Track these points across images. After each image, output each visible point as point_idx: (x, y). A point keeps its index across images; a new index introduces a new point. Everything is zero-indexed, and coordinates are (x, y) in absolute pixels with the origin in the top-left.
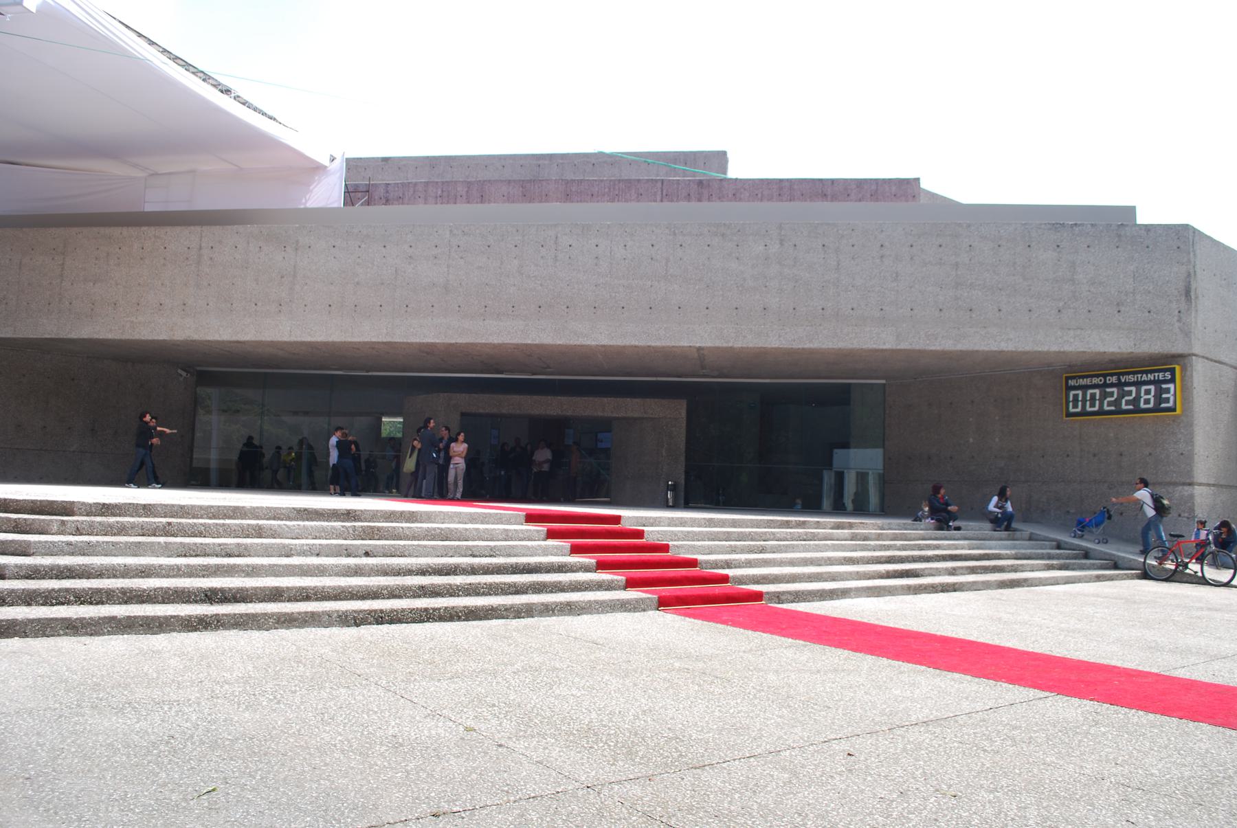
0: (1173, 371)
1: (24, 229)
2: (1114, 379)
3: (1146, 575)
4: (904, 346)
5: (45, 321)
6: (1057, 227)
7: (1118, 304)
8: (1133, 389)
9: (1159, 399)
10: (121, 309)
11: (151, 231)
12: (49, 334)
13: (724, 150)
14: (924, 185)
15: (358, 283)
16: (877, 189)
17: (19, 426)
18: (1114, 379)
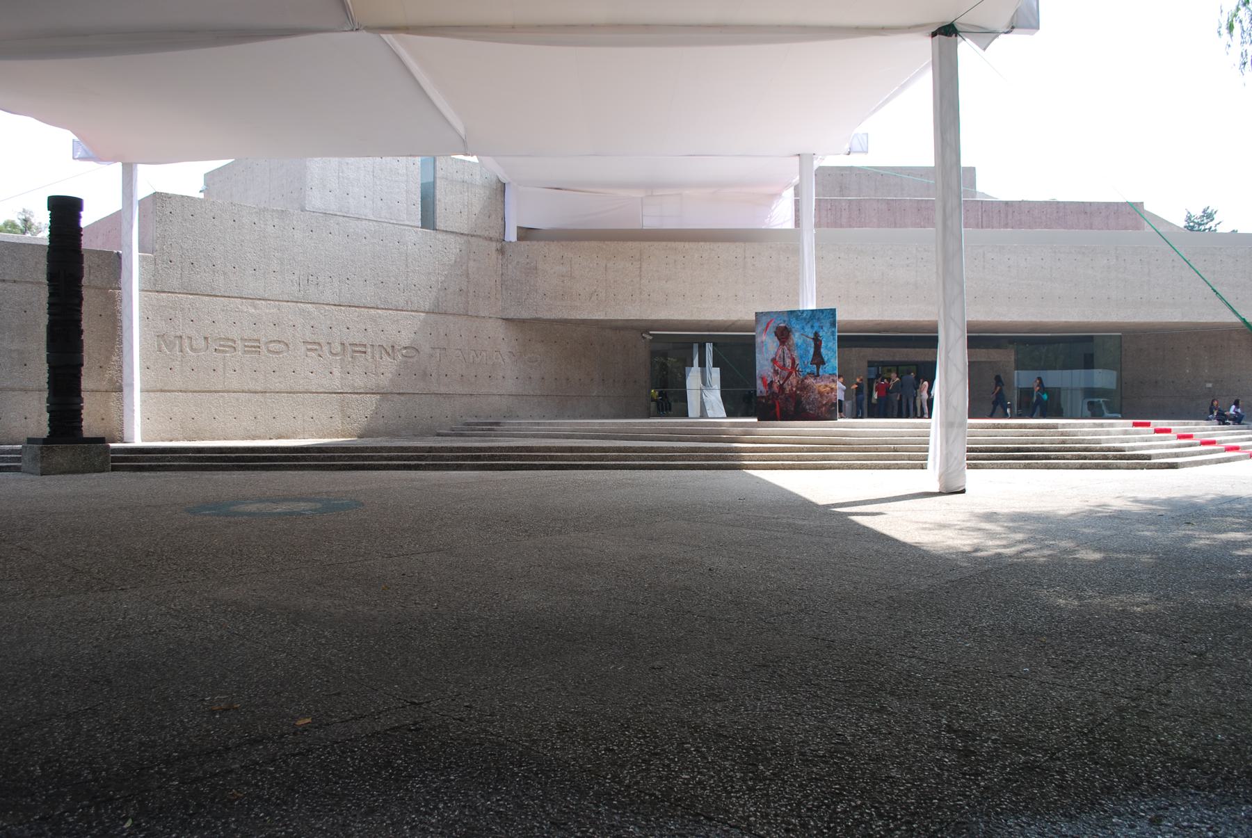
1: (606, 242)
4: (1186, 320)
10: (689, 299)
11: (707, 245)
13: (973, 166)
14: (1147, 207)
16: (1118, 210)
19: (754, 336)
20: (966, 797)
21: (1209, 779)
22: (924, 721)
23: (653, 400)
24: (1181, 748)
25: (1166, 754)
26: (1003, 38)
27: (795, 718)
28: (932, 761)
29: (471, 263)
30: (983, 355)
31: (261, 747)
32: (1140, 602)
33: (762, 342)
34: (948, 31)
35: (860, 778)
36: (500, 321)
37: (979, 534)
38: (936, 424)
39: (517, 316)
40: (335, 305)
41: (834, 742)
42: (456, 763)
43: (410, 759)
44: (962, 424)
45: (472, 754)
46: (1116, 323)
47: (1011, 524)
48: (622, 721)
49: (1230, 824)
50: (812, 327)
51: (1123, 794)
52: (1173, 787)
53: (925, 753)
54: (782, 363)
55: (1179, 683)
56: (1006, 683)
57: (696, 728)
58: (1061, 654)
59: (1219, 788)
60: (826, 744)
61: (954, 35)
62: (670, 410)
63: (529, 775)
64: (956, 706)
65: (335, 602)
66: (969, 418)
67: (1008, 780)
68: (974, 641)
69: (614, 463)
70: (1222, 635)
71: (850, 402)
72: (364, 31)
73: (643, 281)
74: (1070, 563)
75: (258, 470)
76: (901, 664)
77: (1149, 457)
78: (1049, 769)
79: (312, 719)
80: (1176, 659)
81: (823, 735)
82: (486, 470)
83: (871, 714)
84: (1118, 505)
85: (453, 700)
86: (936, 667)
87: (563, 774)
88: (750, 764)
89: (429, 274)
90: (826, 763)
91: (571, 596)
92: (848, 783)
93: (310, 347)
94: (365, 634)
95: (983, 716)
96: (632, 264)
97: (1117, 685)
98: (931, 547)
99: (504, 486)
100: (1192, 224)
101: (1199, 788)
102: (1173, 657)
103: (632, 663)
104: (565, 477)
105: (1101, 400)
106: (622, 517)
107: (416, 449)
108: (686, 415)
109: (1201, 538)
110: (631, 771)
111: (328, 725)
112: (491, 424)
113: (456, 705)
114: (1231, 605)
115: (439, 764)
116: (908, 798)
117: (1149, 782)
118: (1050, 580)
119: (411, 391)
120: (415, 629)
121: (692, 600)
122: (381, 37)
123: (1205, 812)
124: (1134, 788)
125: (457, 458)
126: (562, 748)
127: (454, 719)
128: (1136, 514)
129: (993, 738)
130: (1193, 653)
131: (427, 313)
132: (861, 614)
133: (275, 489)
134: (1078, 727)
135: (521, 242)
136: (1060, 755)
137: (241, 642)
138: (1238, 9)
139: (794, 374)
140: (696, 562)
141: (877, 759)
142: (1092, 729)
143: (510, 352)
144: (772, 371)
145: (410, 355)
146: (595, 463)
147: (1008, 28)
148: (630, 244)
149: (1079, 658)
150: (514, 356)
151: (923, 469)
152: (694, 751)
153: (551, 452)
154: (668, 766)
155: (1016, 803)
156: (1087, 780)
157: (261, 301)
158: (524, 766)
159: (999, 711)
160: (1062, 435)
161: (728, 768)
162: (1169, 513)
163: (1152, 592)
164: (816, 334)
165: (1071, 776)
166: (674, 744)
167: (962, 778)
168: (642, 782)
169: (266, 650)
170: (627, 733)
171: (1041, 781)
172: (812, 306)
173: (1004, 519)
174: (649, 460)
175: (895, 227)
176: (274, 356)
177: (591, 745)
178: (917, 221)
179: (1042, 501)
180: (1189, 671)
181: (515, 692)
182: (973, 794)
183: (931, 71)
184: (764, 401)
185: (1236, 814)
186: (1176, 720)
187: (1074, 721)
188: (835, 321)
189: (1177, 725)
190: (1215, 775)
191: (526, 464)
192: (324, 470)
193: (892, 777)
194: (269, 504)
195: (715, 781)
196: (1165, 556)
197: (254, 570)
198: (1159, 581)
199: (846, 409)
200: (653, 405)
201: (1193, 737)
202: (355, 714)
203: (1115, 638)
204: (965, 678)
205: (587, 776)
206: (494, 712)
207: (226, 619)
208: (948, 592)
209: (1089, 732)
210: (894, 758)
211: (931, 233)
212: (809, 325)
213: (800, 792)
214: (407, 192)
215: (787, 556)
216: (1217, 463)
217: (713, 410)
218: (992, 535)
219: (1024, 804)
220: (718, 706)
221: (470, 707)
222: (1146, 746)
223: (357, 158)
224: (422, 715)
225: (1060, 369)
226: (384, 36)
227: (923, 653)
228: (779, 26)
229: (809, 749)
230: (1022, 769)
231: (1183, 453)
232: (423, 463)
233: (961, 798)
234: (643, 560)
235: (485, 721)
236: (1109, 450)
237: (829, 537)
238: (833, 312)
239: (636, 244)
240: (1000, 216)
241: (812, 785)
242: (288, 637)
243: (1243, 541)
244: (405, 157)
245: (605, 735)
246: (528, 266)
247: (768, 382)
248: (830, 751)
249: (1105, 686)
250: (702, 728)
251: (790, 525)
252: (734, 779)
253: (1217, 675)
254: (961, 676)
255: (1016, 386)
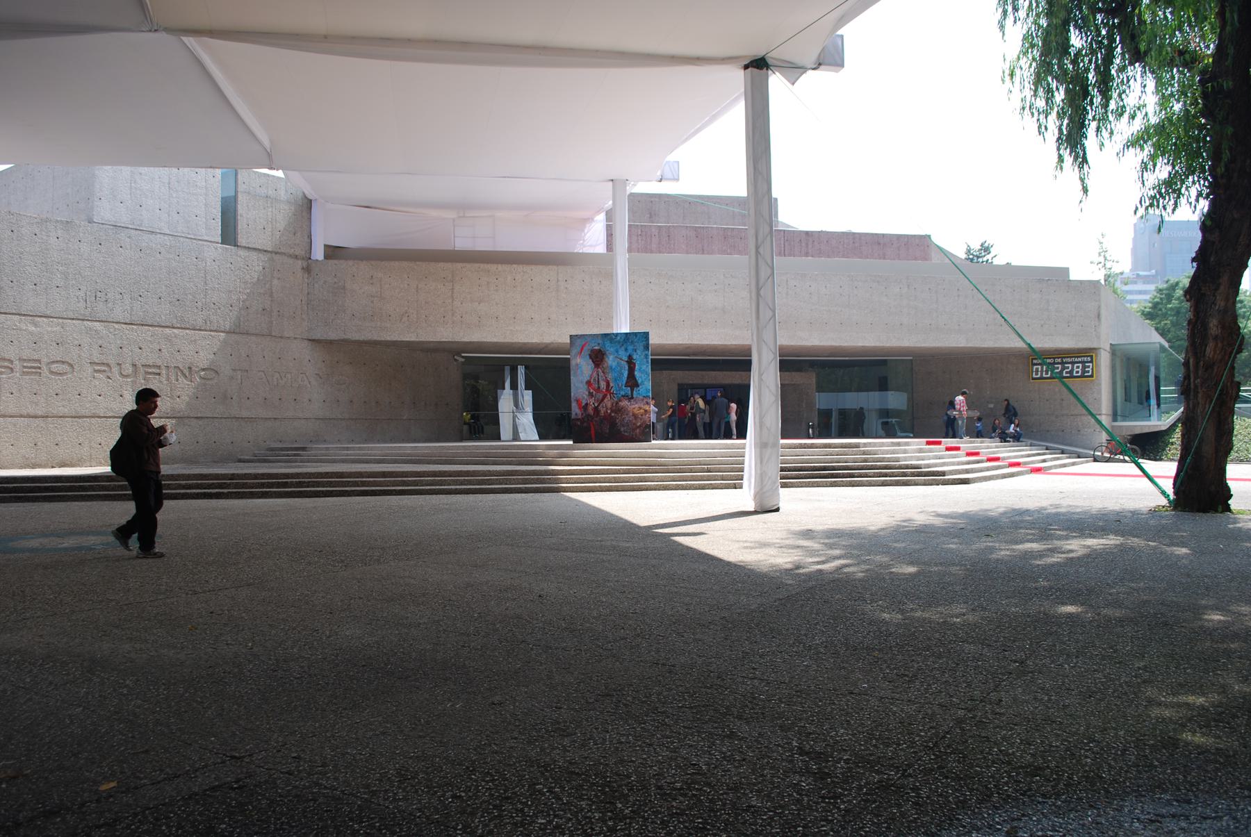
0: (1092, 357)
1: (418, 263)
2: (1059, 360)
3: (1095, 460)
4: (970, 345)
5: (442, 329)
6: (1040, 281)
7: (1068, 322)
8: (1070, 365)
9: (1084, 371)
11: (520, 268)
15: (668, 306)
16: (908, 242)
18: (1059, 360)
19: (569, 358)
20: (829, 822)
21: (1052, 786)
22: (775, 745)
23: (465, 423)
24: (1021, 757)
25: (1009, 763)
26: (810, 72)
27: (646, 749)
28: (791, 786)
29: (275, 282)
30: (797, 378)
31: (59, 819)
32: (958, 613)
33: (577, 365)
34: (759, 64)
35: (721, 810)
36: (306, 342)
37: (799, 552)
38: (751, 445)
39: (324, 337)
40: (126, 324)
41: (689, 772)
42: (288, 823)
43: (235, 822)
44: (775, 445)
45: (306, 812)
46: (908, 347)
47: (827, 541)
48: (466, 764)
49: (1081, 831)
50: (626, 350)
51: (978, 808)
52: (1022, 797)
53: (782, 779)
54: (597, 385)
55: (1008, 692)
56: (848, 701)
57: (546, 766)
58: (895, 668)
59: (1063, 794)
60: (682, 775)
61: (765, 68)
62: (483, 433)
63: (372, 832)
64: (803, 727)
65: (136, 646)
66: (782, 438)
67: (866, 801)
68: (810, 658)
69: (429, 487)
70: (1037, 643)
71: (661, 424)
72: (163, 32)
73: (455, 303)
74: (887, 577)
75: (39, 501)
76: (744, 686)
77: (943, 474)
78: (903, 786)
79: (118, 782)
80: (1001, 668)
81: (678, 766)
82: (294, 497)
83: (722, 741)
84: (921, 519)
85: (279, 751)
86: (779, 688)
87: (410, 827)
88: (607, 803)
89: (230, 292)
90: (685, 795)
91: (397, 629)
92: (710, 816)
93: (97, 368)
94: (173, 681)
95: (832, 736)
96: (444, 285)
97: (952, 696)
98: (755, 565)
99: (315, 514)
100: (971, 257)
101: (1046, 796)
102: (998, 666)
103: (470, 699)
104: (378, 503)
105: (894, 420)
106: (442, 544)
107: (217, 477)
108: (498, 438)
109: (1002, 550)
110: (482, 819)
111: (136, 788)
112: (297, 449)
113: (282, 757)
114: (1040, 612)
115: (269, 826)
116: (772, 828)
117: (998, 793)
118: (871, 595)
119: (210, 415)
120: (229, 673)
121: (526, 629)
122: (181, 39)
123: (1056, 819)
124: (985, 800)
125: (262, 485)
126: (405, 799)
127: (282, 773)
128: (940, 527)
129: (845, 758)
130: (1015, 662)
131: (227, 332)
132: (697, 637)
133: (59, 522)
134: (923, 742)
135: (327, 261)
136: (910, 771)
137: (28, 696)
138: (1019, 58)
139: (609, 396)
140: (525, 588)
141: (735, 788)
142: (936, 742)
143: (316, 374)
144: (587, 393)
145: (209, 377)
146: (409, 488)
147: (815, 64)
148: (441, 265)
149: (912, 671)
150: (321, 378)
151: (736, 488)
152: (547, 791)
153: (363, 478)
154: (522, 810)
155: (878, 824)
156: (941, 795)
157: (42, 319)
158: (364, 822)
159: (846, 729)
160: (864, 454)
161: (585, 808)
162: (969, 527)
163: (967, 603)
164: (630, 357)
165: (926, 792)
166: (524, 786)
167: (822, 802)
168: (495, 830)
169: (58, 704)
170: (473, 777)
171: (898, 800)
172: (625, 329)
173: (819, 536)
174: (465, 485)
175: (703, 253)
176: (57, 378)
177: (436, 792)
178: (724, 248)
179: (853, 518)
180: (1015, 679)
181: (347, 738)
182: (836, 819)
183: (744, 102)
184: (579, 423)
185: (1083, 820)
186: (1012, 729)
187: (919, 735)
188: (648, 344)
189: (1014, 734)
190: (1058, 781)
191: (336, 491)
192: (115, 500)
193: (753, 807)
194: (54, 538)
195: (573, 824)
196: (973, 568)
197: (39, 613)
198: (971, 592)
199: (658, 431)
200: (466, 428)
201: (1030, 745)
202: (168, 774)
203: (941, 650)
204: (808, 697)
205: (435, 829)
206: (325, 763)
207: (9, 671)
208: (778, 611)
209: (934, 746)
210: (752, 786)
211: (741, 262)
212: (623, 348)
213: (663, 829)
214: (206, 205)
215: (616, 579)
216: (1003, 478)
217: (526, 433)
218: (812, 553)
219: (886, 825)
220: (566, 741)
221: (298, 758)
222: (990, 757)
223: (152, 168)
224: (245, 770)
225: (855, 392)
226: (184, 39)
227: (763, 674)
228: (597, 51)
229: (666, 782)
230: (878, 788)
231: (972, 469)
232: (226, 491)
233: (824, 823)
234: (469, 589)
235: (316, 773)
236: (907, 467)
237: (655, 558)
238: (646, 335)
239: (449, 265)
240: (801, 245)
241: (674, 821)
242: (83, 688)
243: (1039, 551)
244: (204, 169)
245: (450, 779)
246: (336, 286)
247: (583, 404)
248: (686, 783)
249: (942, 699)
250: (552, 767)
251: (614, 547)
252: (593, 820)
253: (1040, 681)
254: (804, 695)
255: (817, 407)
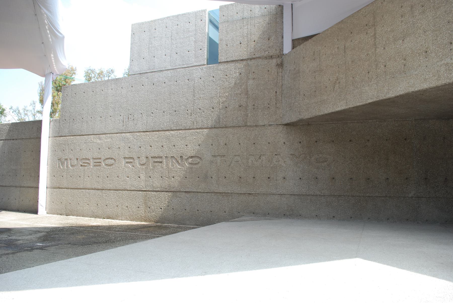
10: (433, 55)
12: (371, 99)
17: (369, 179)
